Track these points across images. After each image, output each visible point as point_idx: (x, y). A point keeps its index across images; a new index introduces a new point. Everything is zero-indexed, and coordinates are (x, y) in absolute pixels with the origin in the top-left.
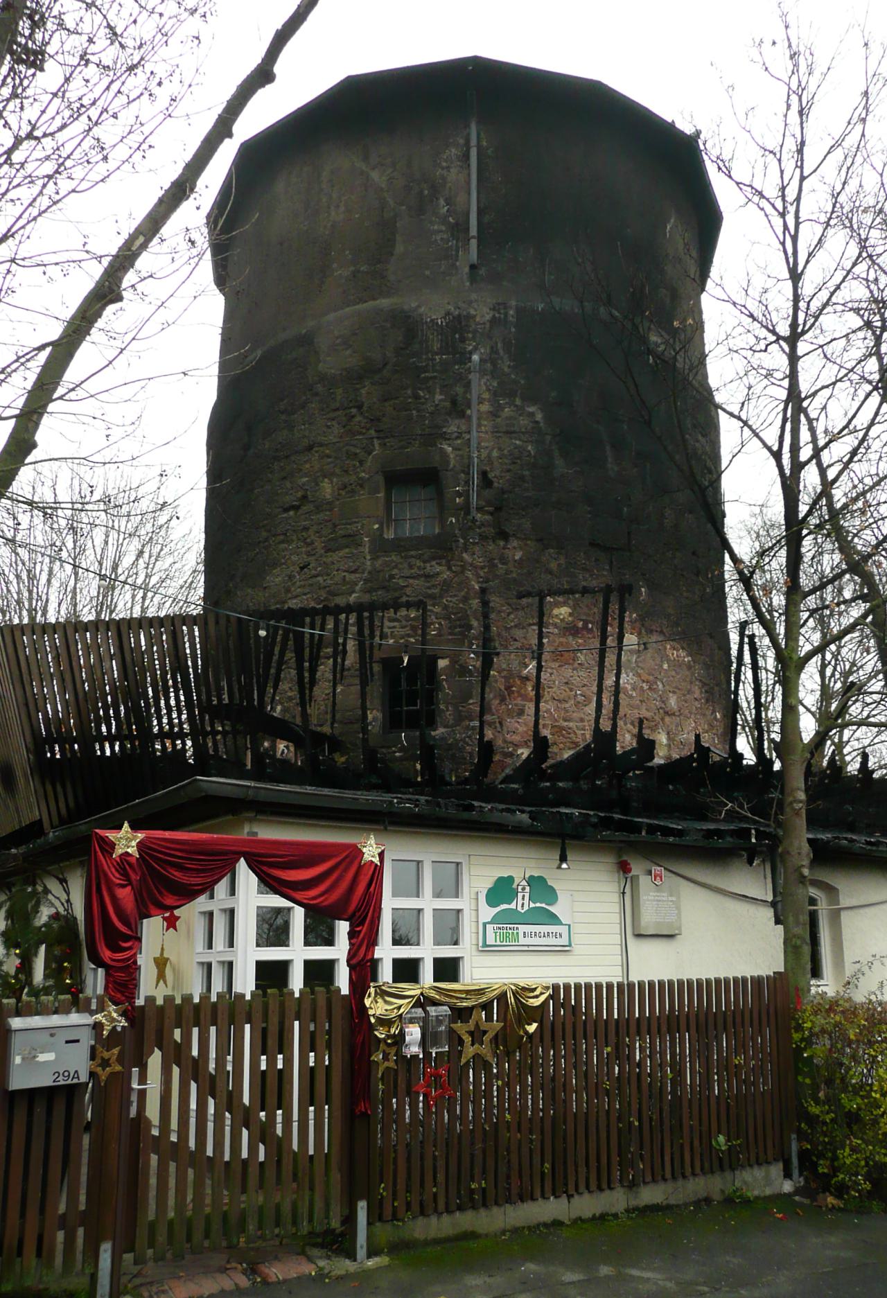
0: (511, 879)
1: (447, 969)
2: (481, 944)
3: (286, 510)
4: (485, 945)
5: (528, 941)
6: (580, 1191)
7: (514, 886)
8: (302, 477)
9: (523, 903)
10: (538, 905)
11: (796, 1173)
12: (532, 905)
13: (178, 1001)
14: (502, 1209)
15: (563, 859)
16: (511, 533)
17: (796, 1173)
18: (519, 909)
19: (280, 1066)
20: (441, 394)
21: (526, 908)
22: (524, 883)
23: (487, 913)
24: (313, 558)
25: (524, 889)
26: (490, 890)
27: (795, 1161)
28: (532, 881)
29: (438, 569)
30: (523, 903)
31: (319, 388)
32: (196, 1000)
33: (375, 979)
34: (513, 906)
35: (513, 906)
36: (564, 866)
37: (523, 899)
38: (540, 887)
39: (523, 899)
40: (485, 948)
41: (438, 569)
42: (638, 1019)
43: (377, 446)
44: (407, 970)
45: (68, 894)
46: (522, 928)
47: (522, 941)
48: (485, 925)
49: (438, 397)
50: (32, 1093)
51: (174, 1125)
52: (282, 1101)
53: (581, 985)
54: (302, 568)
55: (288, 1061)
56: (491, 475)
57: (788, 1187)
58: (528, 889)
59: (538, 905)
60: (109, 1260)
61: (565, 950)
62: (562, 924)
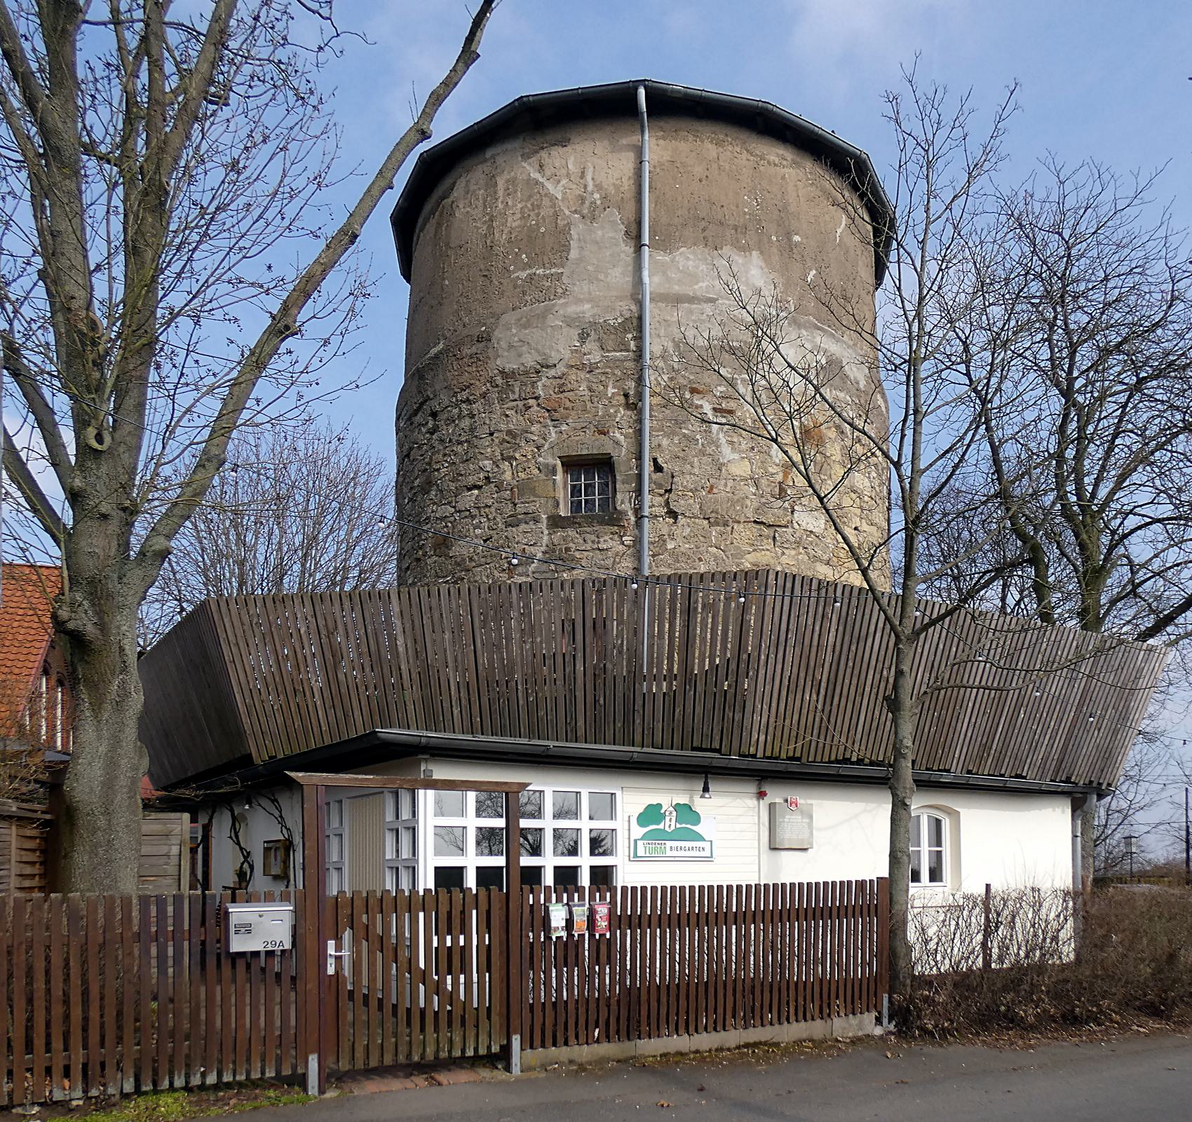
0: (660, 806)
1: (602, 876)
2: (632, 855)
3: (469, 489)
4: (636, 855)
5: (674, 853)
6: (699, 1031)
7: (662, 811)
8: (140, 950)
9: (670, 824)
10: (684, 825)
11: (885, 1021)
12: (678, 826)
13: (379, 895)
14: (633, 1043)
15: (706, 789)
16: (680, 512)
17: (885, 1021)
18: (667, 829)
19: (462, 943)
20: (614, 387)
21: (673, 827)
22: (671, 809)
23: (638, 832)
24: (495, 532)
25: (671, 813)
26: (640, 815)
27: (885, 1011)
28: (677, 807)
29: (611, 543)
30: (670, 824)
31: (499, 380)
32: (407, 894)
33: (539, 883)
34: (661, 826)
35: (661, 826)
36: (707, 796)
37: (670, 820)
38: (687, 813)
39: (670, 820)
40: (635, 857)
41: (611, 543)
42: (736, 913)
43: (553, 435)
44: (566, 876)
45: (280, 812)
46: (669, 844)
47: (669, 853)
48: (636, 841)
49: (611, 391)
50: (242, 954)
51: (379, 985)
52: (465, 969)
53: (769, 885)
54: (485, 541)
55: (468, 940)
56: (660, 460)
57: (878, 1031)
58: (674, 813)
59: (684, 825)
60: (316, 1065)
61: (710, 859)
62: (704, 840)
